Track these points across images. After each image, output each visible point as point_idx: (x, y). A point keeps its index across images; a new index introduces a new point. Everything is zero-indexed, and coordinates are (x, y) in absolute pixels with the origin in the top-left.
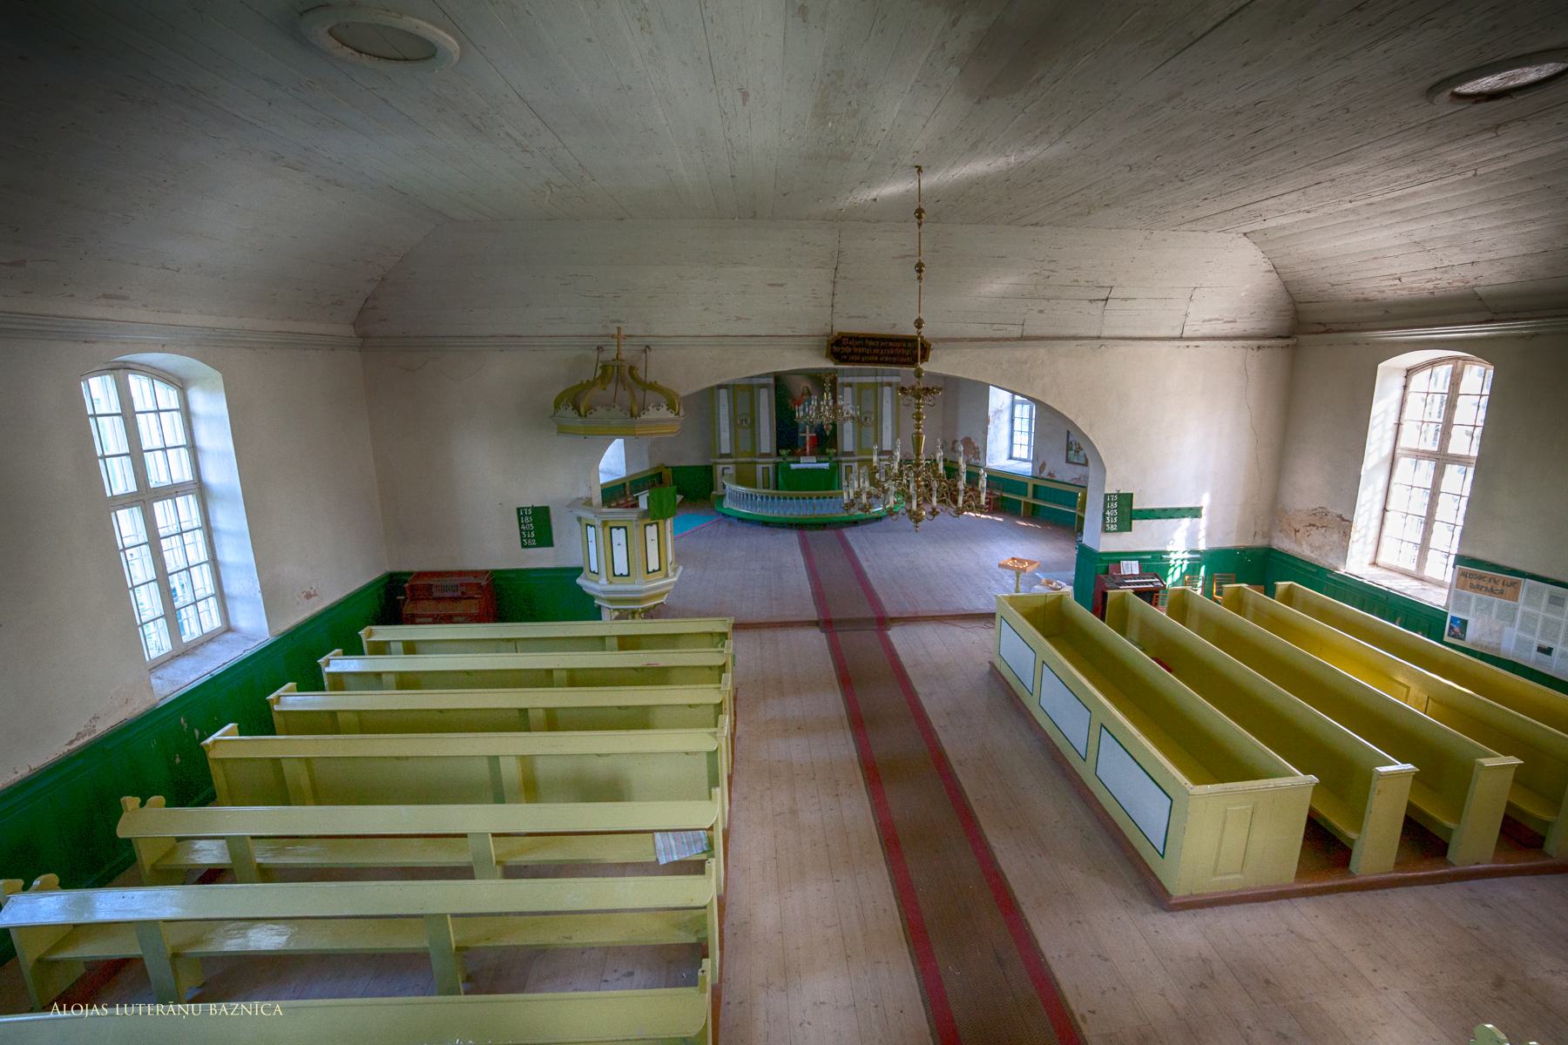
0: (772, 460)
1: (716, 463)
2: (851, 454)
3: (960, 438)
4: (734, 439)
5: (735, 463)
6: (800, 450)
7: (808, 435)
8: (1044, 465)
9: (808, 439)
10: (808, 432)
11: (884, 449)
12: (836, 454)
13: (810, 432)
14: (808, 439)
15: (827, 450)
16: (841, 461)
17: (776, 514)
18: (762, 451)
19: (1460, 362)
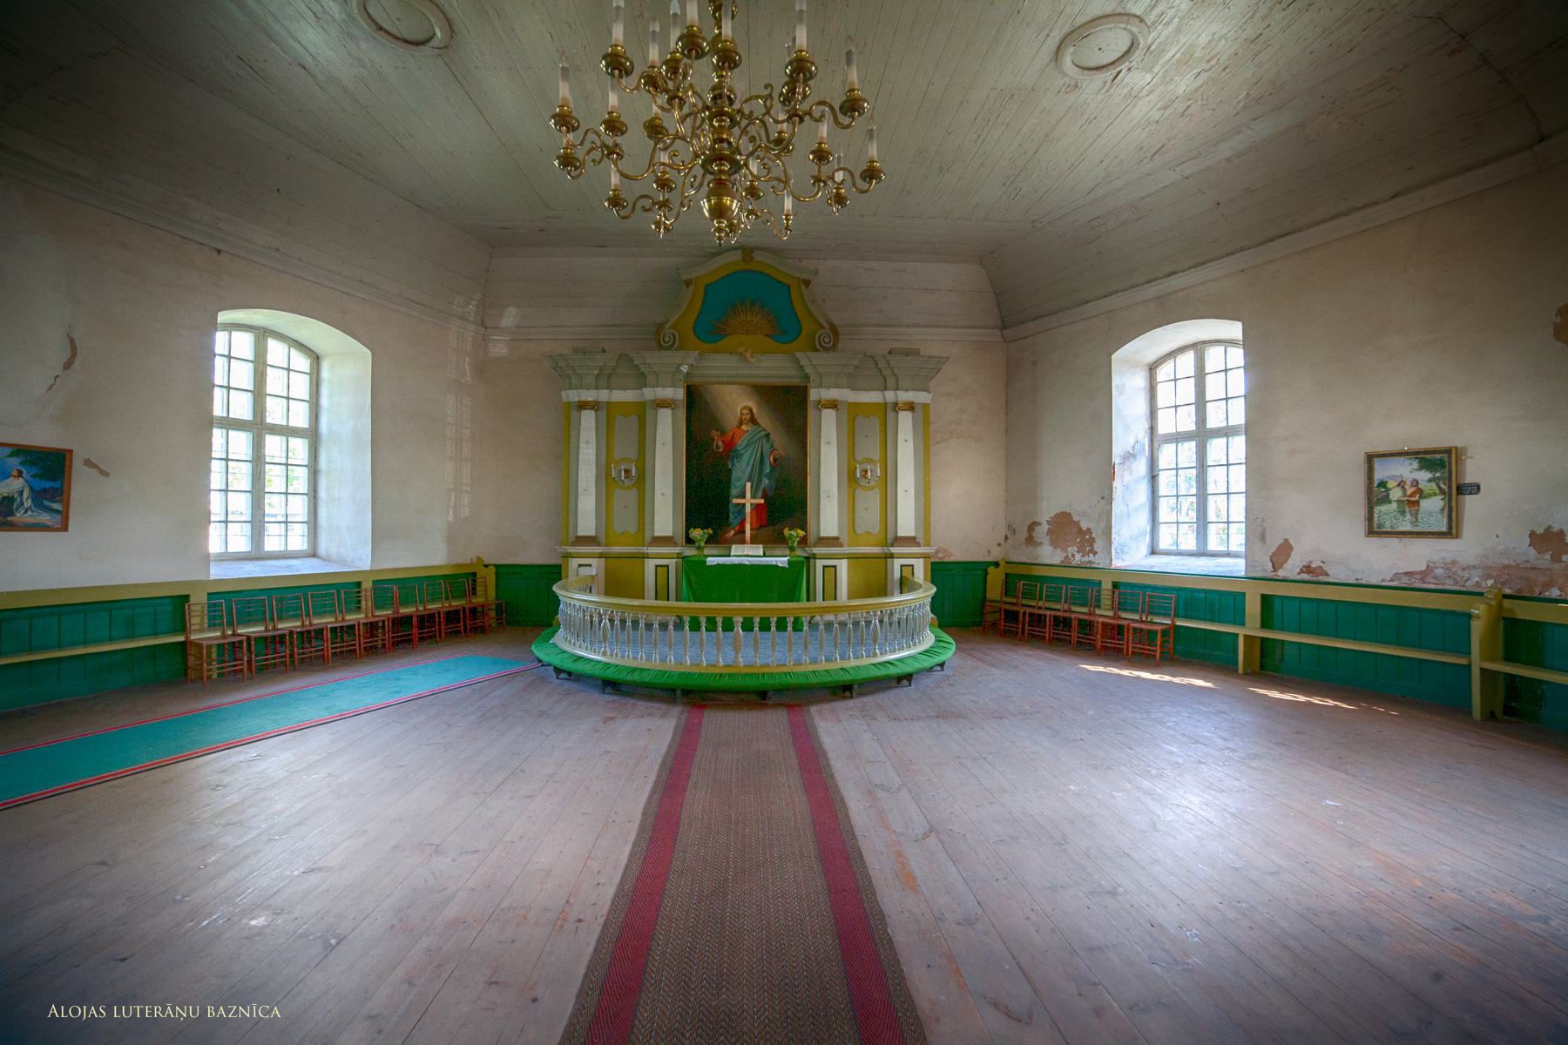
0: (676, 550)
1: (568, 556)
2: (834, 541)
3: (1046, 513)
5: (600, 556)
7: (749, 502)
8: (1285, 550)
9: (748, 509)
10: (748, 495)
11: (899, 535)
12: (804, 541)
13: (753, 497)
14: (748, 509)
15: (786, 532)
16: (815, 557)
17: (655, 663)
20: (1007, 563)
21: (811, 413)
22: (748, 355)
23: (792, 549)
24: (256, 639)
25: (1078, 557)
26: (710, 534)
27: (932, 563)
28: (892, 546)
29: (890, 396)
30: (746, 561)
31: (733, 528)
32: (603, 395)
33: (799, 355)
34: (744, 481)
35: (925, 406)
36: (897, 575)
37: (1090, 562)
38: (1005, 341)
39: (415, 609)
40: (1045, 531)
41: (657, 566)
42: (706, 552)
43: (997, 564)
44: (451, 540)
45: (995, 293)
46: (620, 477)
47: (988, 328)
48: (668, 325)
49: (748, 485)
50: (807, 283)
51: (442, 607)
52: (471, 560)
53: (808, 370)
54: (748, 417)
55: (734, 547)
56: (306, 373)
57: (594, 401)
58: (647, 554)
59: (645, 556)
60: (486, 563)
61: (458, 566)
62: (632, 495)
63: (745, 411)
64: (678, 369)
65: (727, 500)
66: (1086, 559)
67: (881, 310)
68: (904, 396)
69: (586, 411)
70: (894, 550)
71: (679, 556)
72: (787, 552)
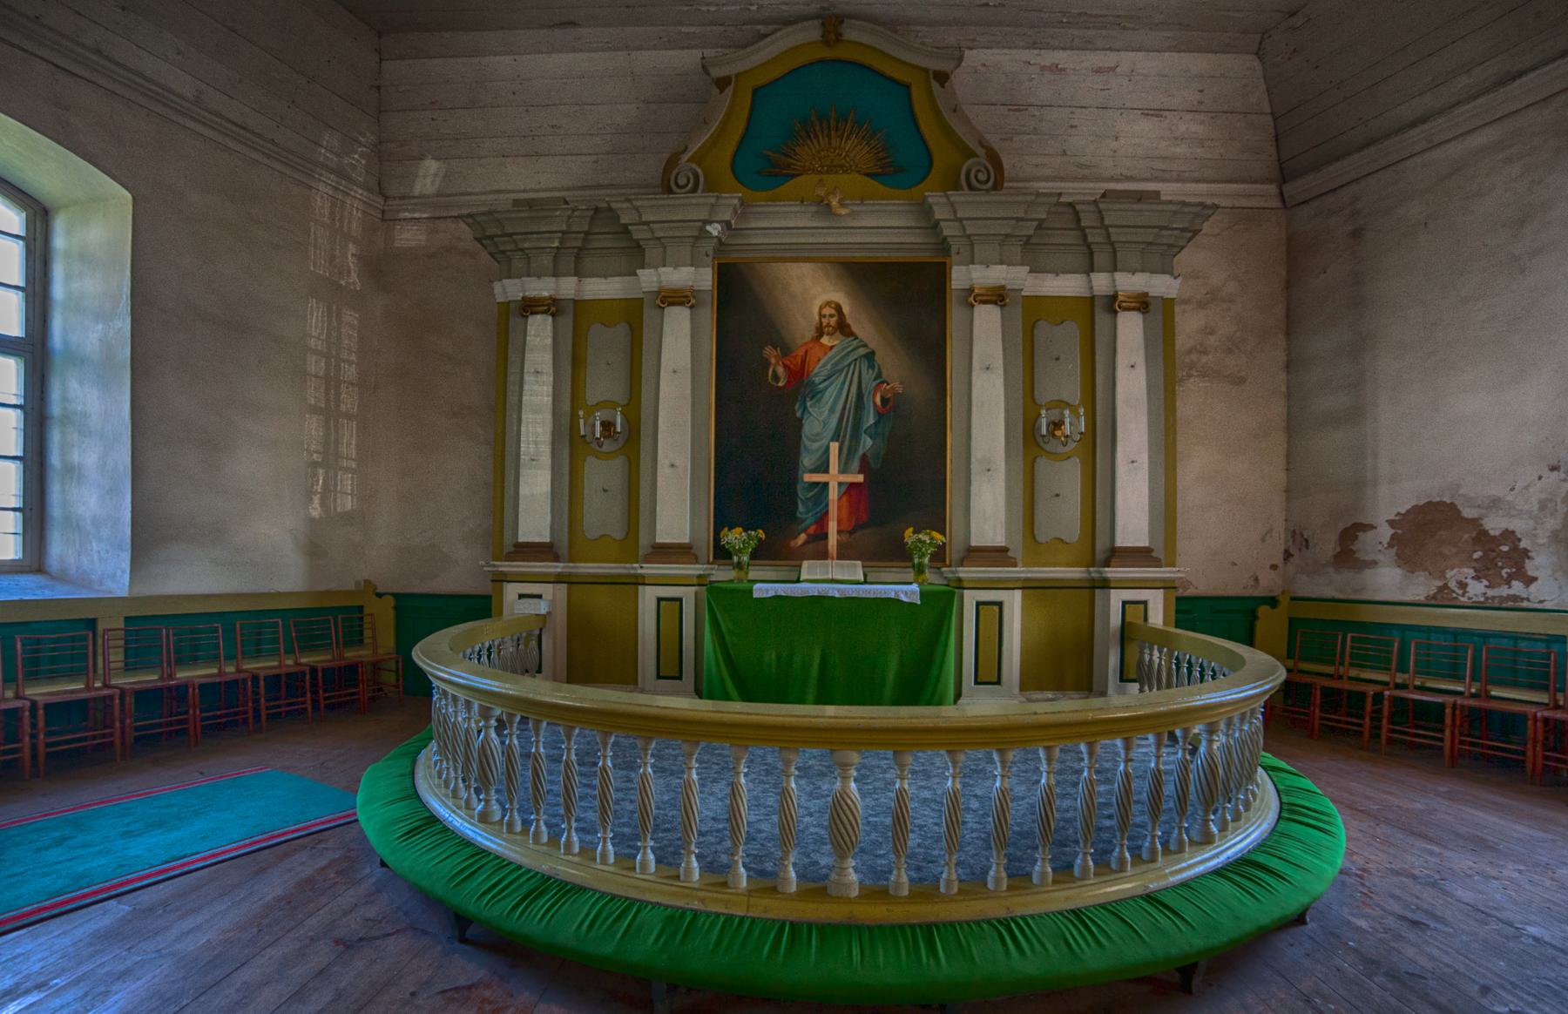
2: (998, 555)
4: (569, 493)
5: (558, 579)
6: (802, 537)
7: (835, 479)
13: (844, 470)
14: (833, 493)
15: (909, 536)
16: (960, 585)
18: (661, 539)
19: (1071, 237)
20: (1293, 599)
21: (955, 314)
22: (834, 203)
23: (920, 570)
24: (47, 706)
25: (1477, 589)
26: (760, 540)
27: (1178, 599)
28: (962, 566)
29: (1101, 282)
30: (834, 591)
31: (805, 531)
32: (567, 287)
33: (934, 198)
34: (825, 441)
35: (1168, 304)
36: (1115, 620)
37: (1515, 598)
38: (1285, 207)
39: (215, 671)
40: (1386, 540)
41: (659, 600)
42: (752, 575)
43: (1272, 602)
44: (314, 550)
45: (1272, 114)
46: (594, 433)
47: (1255, 182)
48: (685, 157)
49: (834, 446)
50: (942, 78)
51: (280, 666)
52: (357, 583)
53: (948, 230)
54: (833, 321)
55: (805, 564)
56: (17, 237)
57: (550, 298)
58: (643, 576)
59: (638, 581)
60: (380, 590)
61: (327, 593)
62: (617, 465)
63: (827, 311)
64: (703, 235)
65: (794, 479)
66: (1504, 591)
67: (1064, 153)
68: (1130, 283)
69: (539, 317)
70: (1112, 572)
71: (701, 581)
72: (911, 575)
